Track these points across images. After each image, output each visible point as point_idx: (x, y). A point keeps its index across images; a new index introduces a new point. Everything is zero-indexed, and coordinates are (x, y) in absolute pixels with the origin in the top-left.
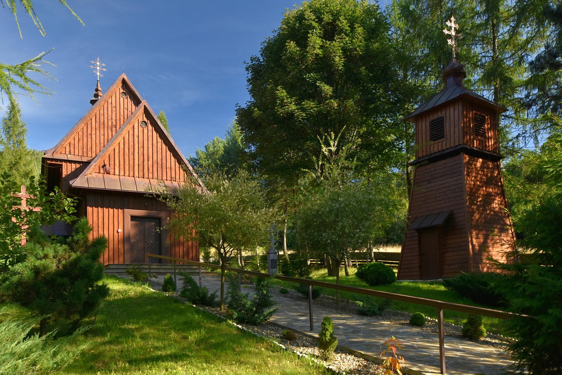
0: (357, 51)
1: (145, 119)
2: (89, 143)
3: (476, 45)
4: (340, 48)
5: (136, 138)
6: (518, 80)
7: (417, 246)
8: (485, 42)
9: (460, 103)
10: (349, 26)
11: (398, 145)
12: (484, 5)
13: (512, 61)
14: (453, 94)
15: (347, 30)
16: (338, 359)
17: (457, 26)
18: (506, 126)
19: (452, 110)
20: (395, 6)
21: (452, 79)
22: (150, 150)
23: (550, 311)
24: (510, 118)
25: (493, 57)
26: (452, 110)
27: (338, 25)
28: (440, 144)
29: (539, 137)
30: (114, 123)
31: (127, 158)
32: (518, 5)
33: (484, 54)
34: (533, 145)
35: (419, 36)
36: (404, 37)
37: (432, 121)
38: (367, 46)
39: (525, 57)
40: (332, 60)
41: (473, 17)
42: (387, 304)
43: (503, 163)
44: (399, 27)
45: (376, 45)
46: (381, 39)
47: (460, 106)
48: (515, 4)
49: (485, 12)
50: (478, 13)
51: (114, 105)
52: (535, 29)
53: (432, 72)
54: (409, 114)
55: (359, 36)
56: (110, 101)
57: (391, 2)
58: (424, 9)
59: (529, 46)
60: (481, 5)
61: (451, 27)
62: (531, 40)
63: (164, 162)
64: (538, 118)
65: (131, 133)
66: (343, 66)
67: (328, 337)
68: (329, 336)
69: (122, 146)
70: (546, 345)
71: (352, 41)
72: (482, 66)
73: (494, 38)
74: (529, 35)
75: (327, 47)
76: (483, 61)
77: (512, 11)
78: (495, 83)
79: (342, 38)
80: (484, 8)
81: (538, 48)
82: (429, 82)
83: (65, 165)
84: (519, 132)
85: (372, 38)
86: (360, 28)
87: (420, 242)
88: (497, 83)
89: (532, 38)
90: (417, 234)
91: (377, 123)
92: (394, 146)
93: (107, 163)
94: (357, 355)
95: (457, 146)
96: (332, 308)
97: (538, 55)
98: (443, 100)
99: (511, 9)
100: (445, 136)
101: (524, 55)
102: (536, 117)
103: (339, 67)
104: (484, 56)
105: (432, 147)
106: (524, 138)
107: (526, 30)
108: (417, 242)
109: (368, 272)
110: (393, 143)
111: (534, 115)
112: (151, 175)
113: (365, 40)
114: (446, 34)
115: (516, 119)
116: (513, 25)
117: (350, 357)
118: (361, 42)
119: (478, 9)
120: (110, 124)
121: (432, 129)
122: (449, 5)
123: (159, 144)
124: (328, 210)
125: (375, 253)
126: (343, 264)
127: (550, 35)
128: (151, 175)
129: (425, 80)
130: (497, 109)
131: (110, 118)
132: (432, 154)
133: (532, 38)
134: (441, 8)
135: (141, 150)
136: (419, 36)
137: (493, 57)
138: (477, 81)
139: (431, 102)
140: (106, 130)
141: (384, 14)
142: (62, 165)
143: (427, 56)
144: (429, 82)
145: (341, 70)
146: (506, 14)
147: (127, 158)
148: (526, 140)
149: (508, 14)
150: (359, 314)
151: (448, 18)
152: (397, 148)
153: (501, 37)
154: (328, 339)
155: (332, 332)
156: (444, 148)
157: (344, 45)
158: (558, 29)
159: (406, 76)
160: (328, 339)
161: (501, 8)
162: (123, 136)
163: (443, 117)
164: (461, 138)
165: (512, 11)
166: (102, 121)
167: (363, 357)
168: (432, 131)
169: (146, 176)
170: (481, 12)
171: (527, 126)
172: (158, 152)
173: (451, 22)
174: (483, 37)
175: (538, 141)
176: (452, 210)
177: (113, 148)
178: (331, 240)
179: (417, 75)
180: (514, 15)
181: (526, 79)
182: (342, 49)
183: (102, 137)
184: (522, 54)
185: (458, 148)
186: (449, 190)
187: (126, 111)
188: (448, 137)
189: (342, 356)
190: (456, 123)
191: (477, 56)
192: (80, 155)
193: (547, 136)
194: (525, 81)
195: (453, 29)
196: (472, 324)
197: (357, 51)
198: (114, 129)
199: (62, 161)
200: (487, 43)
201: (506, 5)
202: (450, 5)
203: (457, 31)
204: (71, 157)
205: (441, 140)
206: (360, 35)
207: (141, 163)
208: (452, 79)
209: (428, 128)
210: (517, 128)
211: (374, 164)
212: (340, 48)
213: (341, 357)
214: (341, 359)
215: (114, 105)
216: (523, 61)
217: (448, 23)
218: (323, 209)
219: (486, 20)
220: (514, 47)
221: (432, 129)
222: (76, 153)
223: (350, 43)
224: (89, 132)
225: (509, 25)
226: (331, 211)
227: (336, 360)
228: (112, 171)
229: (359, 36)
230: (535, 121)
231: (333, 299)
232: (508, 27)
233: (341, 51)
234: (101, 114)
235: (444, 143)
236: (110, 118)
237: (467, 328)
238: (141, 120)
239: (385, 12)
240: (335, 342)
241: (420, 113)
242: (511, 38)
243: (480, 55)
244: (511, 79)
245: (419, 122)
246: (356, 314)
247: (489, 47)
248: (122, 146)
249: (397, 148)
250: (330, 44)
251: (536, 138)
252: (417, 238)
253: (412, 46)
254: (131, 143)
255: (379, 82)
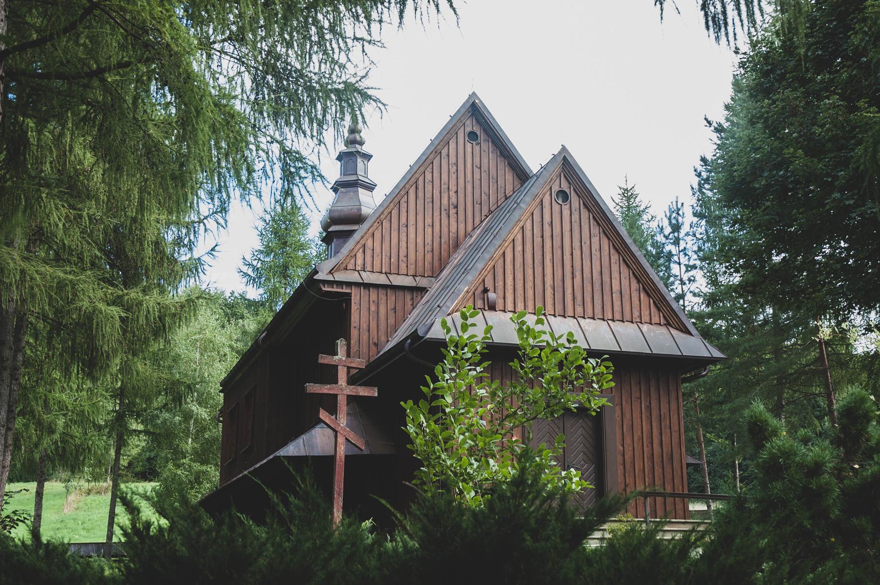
1: (565, 186)
2: (403, 244)
5: (547, 227)
22: (577, 253)
30: (453, 200)
31: (529, 272)
51: (453, 159)
56: (444, 152)
63: (606, 278)
65: (537, 218)
69: (519, 248)
70: (555, 463)
83: (355, 295)
93: (489, 284)
112: (579, 310)
120: (445, 201)
123: (595, 240)
128: (579, 310)
131: (444, 187)
135: (558, 253)
140: (437, 213)
142: (349, 295)
147: (529, 272)
162: (521, 224)
166: (428, 195)
169: (570, 312)
172: (593, 257)
177: (502, 251)
183: (429, 230)
187: (477, 171)
192: (384, 271)
198: (453, 211)
199: (349, 284)
204: (369, 277)
207: (558, 283)
215: (453, 159)
222: (377, 268)
224: (403, 220)
228: (499, 306)
234: (426, 180)
236: (444, 187)
238: (556, 188)
248: (519, 248)
254: (538, 240)
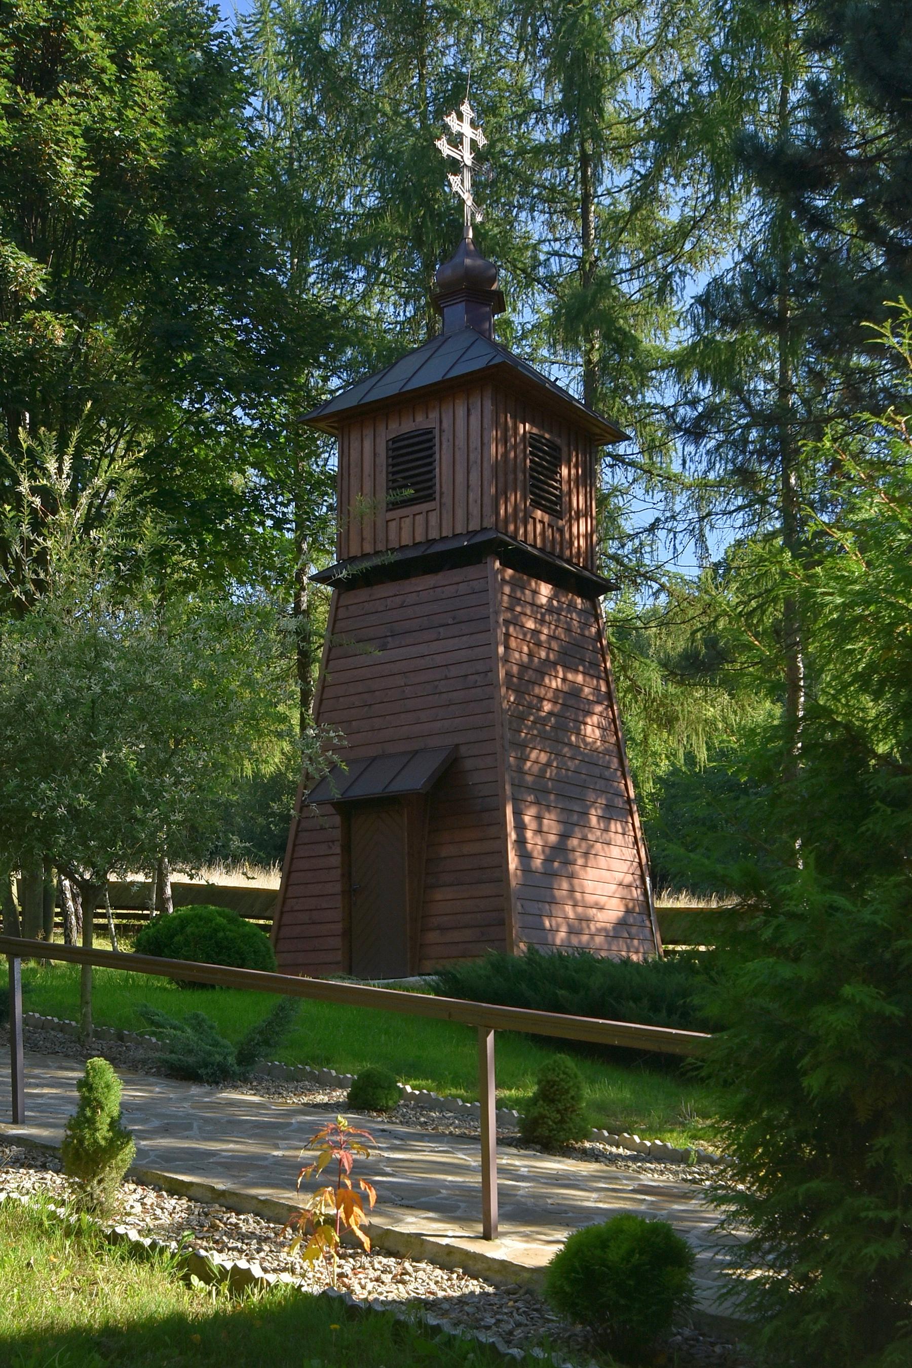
0: (137, 152)
3: (532, 210)
4: (78, 131)
6: (656, 348)
7: (336, 861)
8: (559, 207)
9: (488, 394)
10: (111, 57)
11: (273, 507)
12: (557, 86)
13: (636, 284)
14: (465, 357)
15: (103, 70)
16: (133, 1211)
17: (482, 141)
18: (616, 491)
19: (461, 412)
20: (265, 23)
21: (461, 307)
23: (847, 990)
24: (629, 464)
25: (581, 261)
26: (461, 412)
27: (70, 43)
28: (420, 519)
29: (712, 538)
32: (656, 111)
33: (557, 246)
34: (695, 562)
35: (350, 142)
36: (298, 134)
37: (394, 440)
38: (175, 141)
39: (677, 279)
40: (48, 168)
41: (522, 119)
42: (267, 1043)
43: (607, 605)
44: (278, 98)
45: (208, 145)
46: (223, 128)
47: (489, 406)
48: (647, 104)
49: (561, 110)
50: (535, 108)
52: (704, 196)
53: (389, 273)
54: (314, 403)
55: (146, 100)
57: (249, 8)
58: (366, 57)
59: (688, 246)
60: (546, 85)
61: (460, 135)
62: (693, 227)
64: (712, 476)
66: (86, 195)
67: (103, 1133)
68: (106, 1127)
71: (120, 114)
72: (550, 282)
73: (586, 200)
74: (687, 209)
75: (30, 115)
76: (555, 268)
77: (641, 124)
78: (588, 346)
79: (85, 96)
80: (559, 97)
81: (712, 258)
82: (378, 306)
84: (658, 514)
85: (197, 119)
86: (150, 73)
87: (347, 848)
88: (593, 347)
89: (696, 223)
90: (337, 820)
91: (202, 422)
92: (259, 510)
94: (198, 1195)
95: (476, 532)
96: (67, 1056)
97: (715, 280)
98: (432, 375)
99: (638, 119)
100: (437, 496)
101: (672, 273)
102: (705, 472)
103: (73, 197)
104: (556, 253)
105: (393, 525)
106: (671, 535)
107: (681, 193)
108: (338, 850)
109: (179, 938)
110: (256, 498)
111: (703, 466)
113: (172, 120)
114: (445, 155)
115: (645, 472)
116: (643, 172)
117: (173, 1202)
118: (153, 121)
119: (538, 94)
121: (393, 466)
122: (449, 60)
124: (58, 698)
125: (174, 886)
126: (57, 925)
127: (747, 224)
129: (365, 296)
130: (598, 431)
132: (431, 542)
133: (696, 223)
134: (423, 65)
136: (350, 142)
137: (581, 261)
138: (530, 331)
139: (389, 378)
141: (235, 41)
143: (374, 214)
144: (378, 306)
145: (79, 211)
146: (621, 130)
148: (677, 542)
149: (628, 132)
150: (168, 1076)
151: (451, 103)
152: (272, 517)
153: (606, 201)
154: (105, 1138)
155: (115, 1114)
156: (434, 534)
157: (95, 122)
158: (771, 211)
159: (301, 274)
160: (105, 1138)
161: (609, 107)
163: (430, 431)
164: (488, 509)
165: (641, 124)
167: (222, 1200)
168: (394, 473)
170: (548, 107)
171: (678, 498)
173: (460, 117)
174: (552, 189)
175: (707, 549)
176: (457, 746)
178: (69, 808)
179: (338, 276)
180: (645, 140)
181: (677, 348)
182: (87, 133)
184: (665, 268)
185: (479, 539)
186: (446, 678)
188: (447, 500)
189: (148, 1201)
190: (472, 457)
191: (535, 247)
193: (731, 537)
194: (673, 356)
195: (467, 143)
196: (553, 1101)
197: (137, 152)
200: (565, 211)
201: (623, 102)
202: (451, 62)
203: (480, 156)
205: (425, 507)
206: (151, 99)
208: (461, 307)
209: (382, 459)
210: (648, 498)
211: (186, 563)
212: (78, 131)
213: (143, 1204)
214: (145, 1211)
216: (672, 289)
217: (451, 121)
218: (40, 693)
219: (562, 136)
220: (644, 242)
221: (393, 466)
223: (113, 119)
225: (631, 165)
226: (70, 704)
227: (129, 1214)
229: (146, 100)
230: (704, 484)
231: (62, 1028)
232: (627, 175)
233: (81, 141)
235: (433, 519)
237: (535, 1112)
239: (238, 34)
240: (127, 1150)
241: (399, 394)
242: (635, 209)
243: (545, 248)
244: (636, 343)
245: (352, 437)
246: (158, 1074)
247: (570, 225)
249: (272, 517)
250: (41, 108)
251: (701, 540)
252: (337, 834)
253: (324, 173)
255: (213, 279)
